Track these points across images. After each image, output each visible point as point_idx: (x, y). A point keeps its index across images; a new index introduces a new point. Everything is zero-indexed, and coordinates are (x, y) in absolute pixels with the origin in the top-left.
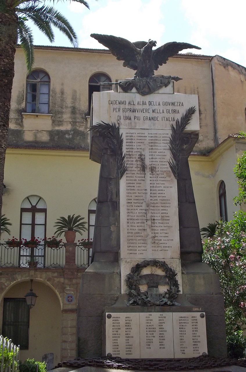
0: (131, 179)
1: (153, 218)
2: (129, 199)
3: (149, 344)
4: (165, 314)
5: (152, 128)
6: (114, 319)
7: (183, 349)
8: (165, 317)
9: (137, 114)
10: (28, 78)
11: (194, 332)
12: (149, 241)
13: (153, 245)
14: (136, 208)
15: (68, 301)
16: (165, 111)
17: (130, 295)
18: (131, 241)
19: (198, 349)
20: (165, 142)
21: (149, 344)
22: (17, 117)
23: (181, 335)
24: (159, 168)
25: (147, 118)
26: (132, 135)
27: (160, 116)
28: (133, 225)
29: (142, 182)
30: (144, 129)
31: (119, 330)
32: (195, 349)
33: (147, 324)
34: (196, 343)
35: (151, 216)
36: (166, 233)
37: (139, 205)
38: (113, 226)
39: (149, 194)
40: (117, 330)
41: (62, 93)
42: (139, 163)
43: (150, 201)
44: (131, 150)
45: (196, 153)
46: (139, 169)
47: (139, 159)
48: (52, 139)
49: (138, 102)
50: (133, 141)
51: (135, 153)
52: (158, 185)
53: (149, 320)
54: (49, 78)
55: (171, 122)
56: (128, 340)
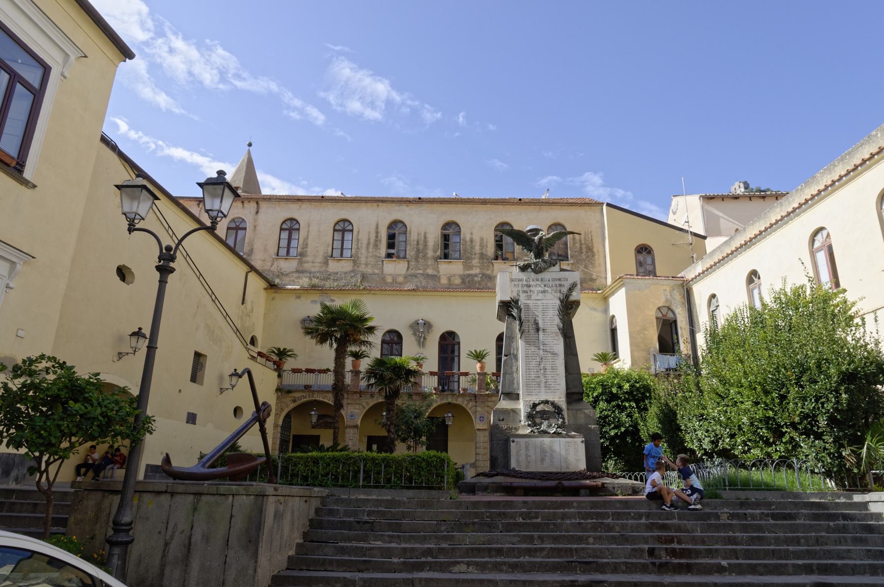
5: (544, 298)
9: (532, 289)
10: (442, 229)
12: (543, 385)
15: (480, 421)
16: (554, 286)
41: (472, 241)
42: (534, 326)
48: (463, 282)
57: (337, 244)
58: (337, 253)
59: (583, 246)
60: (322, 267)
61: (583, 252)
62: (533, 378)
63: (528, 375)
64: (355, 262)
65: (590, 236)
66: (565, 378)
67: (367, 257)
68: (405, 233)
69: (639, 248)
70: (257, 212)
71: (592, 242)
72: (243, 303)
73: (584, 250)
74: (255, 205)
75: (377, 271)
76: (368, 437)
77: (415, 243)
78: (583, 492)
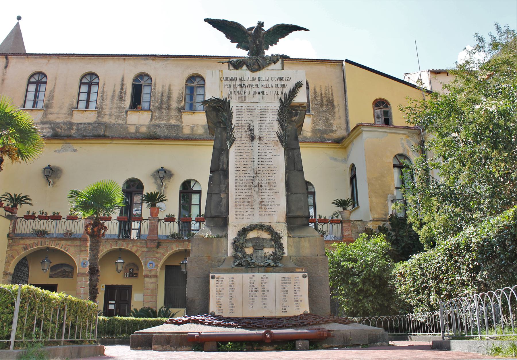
0: (240, 148)
1: (260, 184)
3: (251, 303)
4: (267, 275)
5: (262, 100)
7: (285, 308)
8: (267, 278)
9: (247, 89)
10: (186, 82)
12: (256, 206)
13: (260, 210)
14: (244, 175)
16: (274, 86)
18: (238, 207)
20: (273, 113)
21: (251, 303)
26: (242, 108)
27: (269, 90)
28: (241, 191)
30: (254, 102)
37: (247, 172)
42: (248, 133)
43: (258, 169)
44: (240, 122)
46: (248, 139)
47: (248, 130)
50: (243, 116)
51: (245, 125)
52: (266, 154)
53: (252, 281)
54: (204, 81)
56: (231, 299)
57: (83, 97)
58: (82, 105)
60: (67, 118)
61: (323, 105)
64: (99, 114)
65: (330, 90)
66: (285, 197)
67: (111, 109)
68: (150, 85)
70: (6, 67)
73: (325, 103)
74: (5, 60)
75: (120, 122)
76: (106, 285)
77: (160, 95)
78: (299, 343)
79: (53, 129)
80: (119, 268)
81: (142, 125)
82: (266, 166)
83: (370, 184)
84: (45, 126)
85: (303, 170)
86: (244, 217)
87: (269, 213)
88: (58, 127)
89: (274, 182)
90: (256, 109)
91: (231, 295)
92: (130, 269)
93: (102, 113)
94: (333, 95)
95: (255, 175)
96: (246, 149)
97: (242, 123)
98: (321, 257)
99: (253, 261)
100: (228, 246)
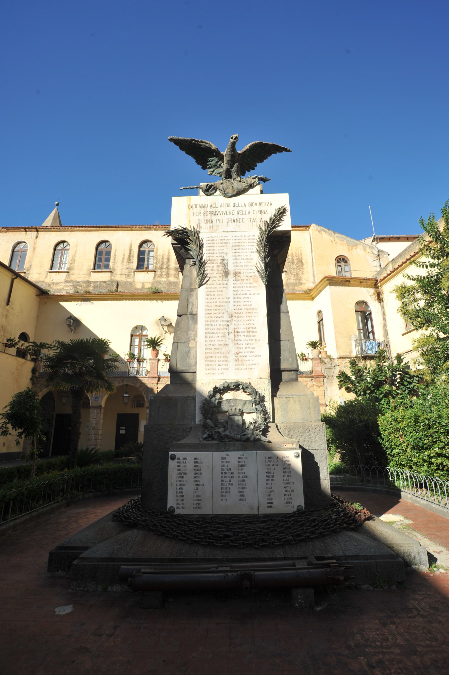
1: (236, 330)
2: (208, 310)
3: (224, 494)
4: (246, 453)
6: (179, 461)
7: (271, 501)
8: (246, 458)
9: (219, 217)
11: (286, 478)
12: (232, 357)
13: (237, 363)
14: (216, 319)
16: (251, 212)
17: (205, 426)
18: (209, 359)
19: (290, 501)
20: (252, 244)
21: (224, 494)
22: (175, 273)
23: (268, 482)
24: (245, 273)
25: (231, 220)
26: (214, 238)
27: (245, 217)
28: (212, 339)
29: (224, 290)
30: (227, 232)
31: (185, 476)
32: (286, 501)
33: (222, 468)
34: (288, 493)
35: (234, 328)
36: (252, 348)
37: (219, 315)
38: (192, 341)
39: (231, 304)
40: (182, 475)
42: (220, 268)
43: (234, 311)
44: (212, 255)
45: (301, 292)
46: (220, 275)
47: (221, 265)
49: (221, 205)
50: (215, 248)
51: (217, 258)
52: (242, 293)
53: (225, 462)
55: (258, 223)
56: (197, 489)
59: (295, 258)
60: (86, 277)
62: (217, 346)
63: (209, 343)
69: (337, 259)
70: (37, 237)
71: (301, 256)
72: (8, 304)
73: (295, 261)
75: (129, 280)
77: (161, 257)
79: (75, 286)
80: (126, 401)
81: (146, 282)
82: (243, 308)
83: (336, 327)
84: (68, 284)
85: (288, 312)
86: (217, 371)
87: (248, 366)
88: (79, 285)
89: (253, 326)
90: (230, 240)
91: (196, 483)
92: (138, 400)
93: (115, 273)
94: (302, 254)
95: (230, 319)
96: (218, 288)
97: (213, 257)
98: (315, 424)
99: (227, 433)
100: (195, 410)
